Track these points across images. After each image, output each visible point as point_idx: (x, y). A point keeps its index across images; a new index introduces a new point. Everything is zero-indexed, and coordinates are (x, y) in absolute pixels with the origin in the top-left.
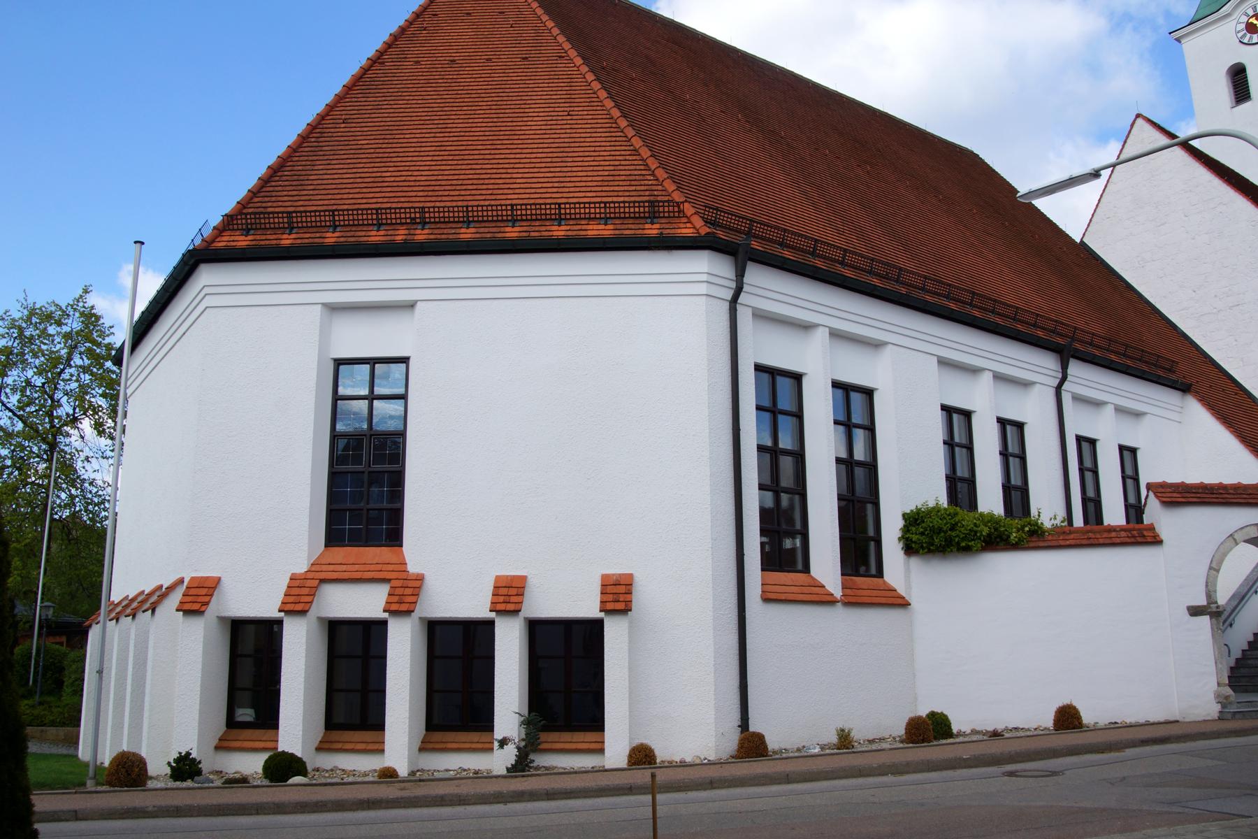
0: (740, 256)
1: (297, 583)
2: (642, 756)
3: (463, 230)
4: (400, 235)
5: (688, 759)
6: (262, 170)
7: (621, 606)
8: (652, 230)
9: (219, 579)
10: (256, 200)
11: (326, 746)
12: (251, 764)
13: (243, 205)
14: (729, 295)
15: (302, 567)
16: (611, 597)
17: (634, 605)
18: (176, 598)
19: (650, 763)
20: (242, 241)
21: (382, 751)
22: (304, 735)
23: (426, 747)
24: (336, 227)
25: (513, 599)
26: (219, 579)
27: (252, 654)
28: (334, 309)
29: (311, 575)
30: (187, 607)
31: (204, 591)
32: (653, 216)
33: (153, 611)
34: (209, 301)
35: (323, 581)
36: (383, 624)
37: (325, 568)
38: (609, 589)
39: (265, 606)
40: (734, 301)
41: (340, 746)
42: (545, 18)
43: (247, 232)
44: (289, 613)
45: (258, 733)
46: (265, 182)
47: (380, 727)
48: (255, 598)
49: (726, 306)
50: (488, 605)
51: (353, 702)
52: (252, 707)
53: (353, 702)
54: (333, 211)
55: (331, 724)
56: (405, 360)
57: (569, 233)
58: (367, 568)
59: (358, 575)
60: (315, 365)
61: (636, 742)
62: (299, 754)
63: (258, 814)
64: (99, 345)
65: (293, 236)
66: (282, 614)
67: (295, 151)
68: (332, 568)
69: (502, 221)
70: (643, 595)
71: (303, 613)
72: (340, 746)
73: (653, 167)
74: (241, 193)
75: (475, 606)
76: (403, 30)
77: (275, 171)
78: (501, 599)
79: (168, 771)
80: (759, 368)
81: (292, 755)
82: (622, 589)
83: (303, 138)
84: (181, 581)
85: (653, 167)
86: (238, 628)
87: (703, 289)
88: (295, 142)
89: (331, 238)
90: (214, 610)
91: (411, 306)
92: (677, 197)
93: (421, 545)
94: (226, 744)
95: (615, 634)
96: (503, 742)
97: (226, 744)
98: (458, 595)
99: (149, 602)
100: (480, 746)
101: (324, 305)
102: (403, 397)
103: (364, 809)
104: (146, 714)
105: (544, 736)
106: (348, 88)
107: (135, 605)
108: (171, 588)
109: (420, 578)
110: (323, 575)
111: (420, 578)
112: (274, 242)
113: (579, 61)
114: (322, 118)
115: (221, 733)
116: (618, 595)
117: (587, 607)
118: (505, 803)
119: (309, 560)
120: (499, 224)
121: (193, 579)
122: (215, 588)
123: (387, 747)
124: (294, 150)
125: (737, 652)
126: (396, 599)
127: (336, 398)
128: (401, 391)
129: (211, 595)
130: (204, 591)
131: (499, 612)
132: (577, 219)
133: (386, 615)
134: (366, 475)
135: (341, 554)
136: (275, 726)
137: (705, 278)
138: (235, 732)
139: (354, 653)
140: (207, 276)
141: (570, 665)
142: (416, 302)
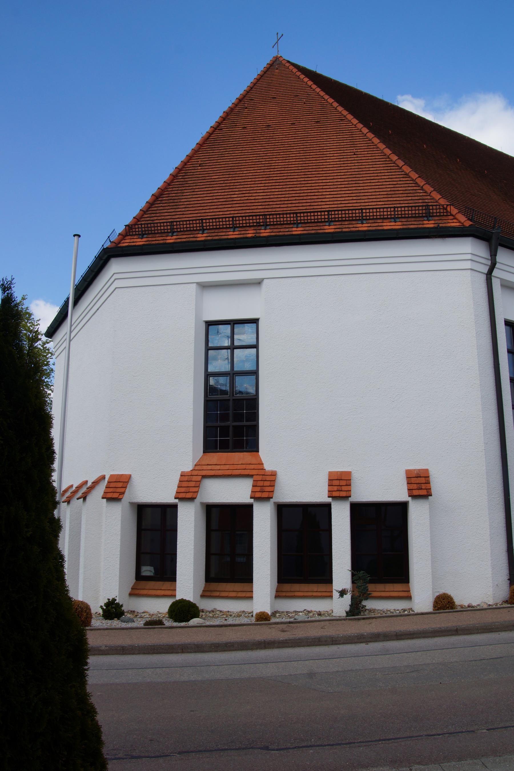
0: (493, 242)
1: (186, 478)
2: (444, 603)
3: (294, 229)
4: (250, 233)
5: (474, 604)
6: (148, 197)
7: (424, 492)
8: (430, 224)
9: (130, 477)
10: (146, 216)
11: (208, 594)
12: (160, 606)
13: (137, 219)
14: (485, 270)
15: (188, 467)
16: (415, 486)
17: (433, 491)
18: (101, 489)
19: (452, 608)
20: (140, 242)
21: (251, 598)
22: (194, 587)
23: (279, 595)
24: (204, 230)
25: (344, 488)
26: (130, 477)
27: (154, 528)
28: (204, 286)
29: (196, 473)
30: (109, 495)
31: (120, 485)
32: (428, 216)
33: (85, 498)
34: (117, 284)
35: (204, 477)
36: (174, 507)
37: (205, 467)
38: (413, 480)
39: (166, 495)
40: (489, 275)
41: (218, 594)
42: (327, 97)
43: (142, 236)
44: (181, 499)
45: (158, 584)
46: (151, 205)
47: (250, 580)
48: (156, 488)
49: (484, 277)
50: (174, 493)
51: (228, 564)
52: (151, 566)
53: (228, 564)
54: (202, 220)
55: (208, 579)
56: (255, 321)
57: (371, 228)
58: (236, 467)
59: (229, 472)
60: (193, 325)
61: (442, 591)
62: (192, 600)
63: (183, 652)
64: (31, 331)
65: (174, 237)
66: (177, 501)
67: (169, 185)
68: (209, 467)
69: (321, 222)
70: (437, 484)
71: (192, 499)
72: (218, 594)
73: (422, 184)
74: (136, 212)
75: (316, 493)
76: (231, 109)
77: (157, 198)
78: (335, 488)
79: (101, 611)
80: (508, 323)
81: (189, 602)
82: (423, 480)
83: (174, 177)
84: (103, 478)
85: (422, 184)
86: (142, 510)
87: (468, 265)
88: (168, 179)
89: (201, 237)
90: (127, 498)
91: (259, 283)
92: (443, 202)
93: (271, 450)
94: (137, 592)
95: (418, 515)
96: (342, 593)
97: (137, 592)
98: (303, 487)
99: (84, 492)
100: (319, 594)
101: (198, 283)
102: (256, 346)
103: (261, 648)
104: (81, 571)
105: (371, 587)
106: (200, 145)
107: (68, 494)
108: (96, 483)
109: (274, 474)
110: (204, 473)
111: (274, 474)
112: (162, 242)
113: (355, 121)
114: (185, 164)
115: (132, 584)
116: (420, 485)
117: (398, 493)
118: (367, 642)
119: (193, 462)
120: (319, 224)
121: (112, 476)
122: (127, 482)
123: (255, 595)
124: (168, 184)
125: (504, 525)
126: (258, 489)
127: (208, 349)
128: (253, 342)
129: (126, 487)
130: (120, 485)
131: (334, 498)
132: (375, 219)
133: (252, 501)
134: (231, 403)
135: (215, 457)
136: (173, 579)
137: (469, 257)
138: (143, 583)
139: (228, 527)
140: (116, 267)
141: (383, 536)
142: (263, 280)
